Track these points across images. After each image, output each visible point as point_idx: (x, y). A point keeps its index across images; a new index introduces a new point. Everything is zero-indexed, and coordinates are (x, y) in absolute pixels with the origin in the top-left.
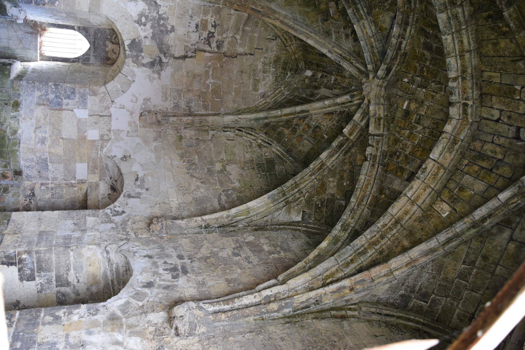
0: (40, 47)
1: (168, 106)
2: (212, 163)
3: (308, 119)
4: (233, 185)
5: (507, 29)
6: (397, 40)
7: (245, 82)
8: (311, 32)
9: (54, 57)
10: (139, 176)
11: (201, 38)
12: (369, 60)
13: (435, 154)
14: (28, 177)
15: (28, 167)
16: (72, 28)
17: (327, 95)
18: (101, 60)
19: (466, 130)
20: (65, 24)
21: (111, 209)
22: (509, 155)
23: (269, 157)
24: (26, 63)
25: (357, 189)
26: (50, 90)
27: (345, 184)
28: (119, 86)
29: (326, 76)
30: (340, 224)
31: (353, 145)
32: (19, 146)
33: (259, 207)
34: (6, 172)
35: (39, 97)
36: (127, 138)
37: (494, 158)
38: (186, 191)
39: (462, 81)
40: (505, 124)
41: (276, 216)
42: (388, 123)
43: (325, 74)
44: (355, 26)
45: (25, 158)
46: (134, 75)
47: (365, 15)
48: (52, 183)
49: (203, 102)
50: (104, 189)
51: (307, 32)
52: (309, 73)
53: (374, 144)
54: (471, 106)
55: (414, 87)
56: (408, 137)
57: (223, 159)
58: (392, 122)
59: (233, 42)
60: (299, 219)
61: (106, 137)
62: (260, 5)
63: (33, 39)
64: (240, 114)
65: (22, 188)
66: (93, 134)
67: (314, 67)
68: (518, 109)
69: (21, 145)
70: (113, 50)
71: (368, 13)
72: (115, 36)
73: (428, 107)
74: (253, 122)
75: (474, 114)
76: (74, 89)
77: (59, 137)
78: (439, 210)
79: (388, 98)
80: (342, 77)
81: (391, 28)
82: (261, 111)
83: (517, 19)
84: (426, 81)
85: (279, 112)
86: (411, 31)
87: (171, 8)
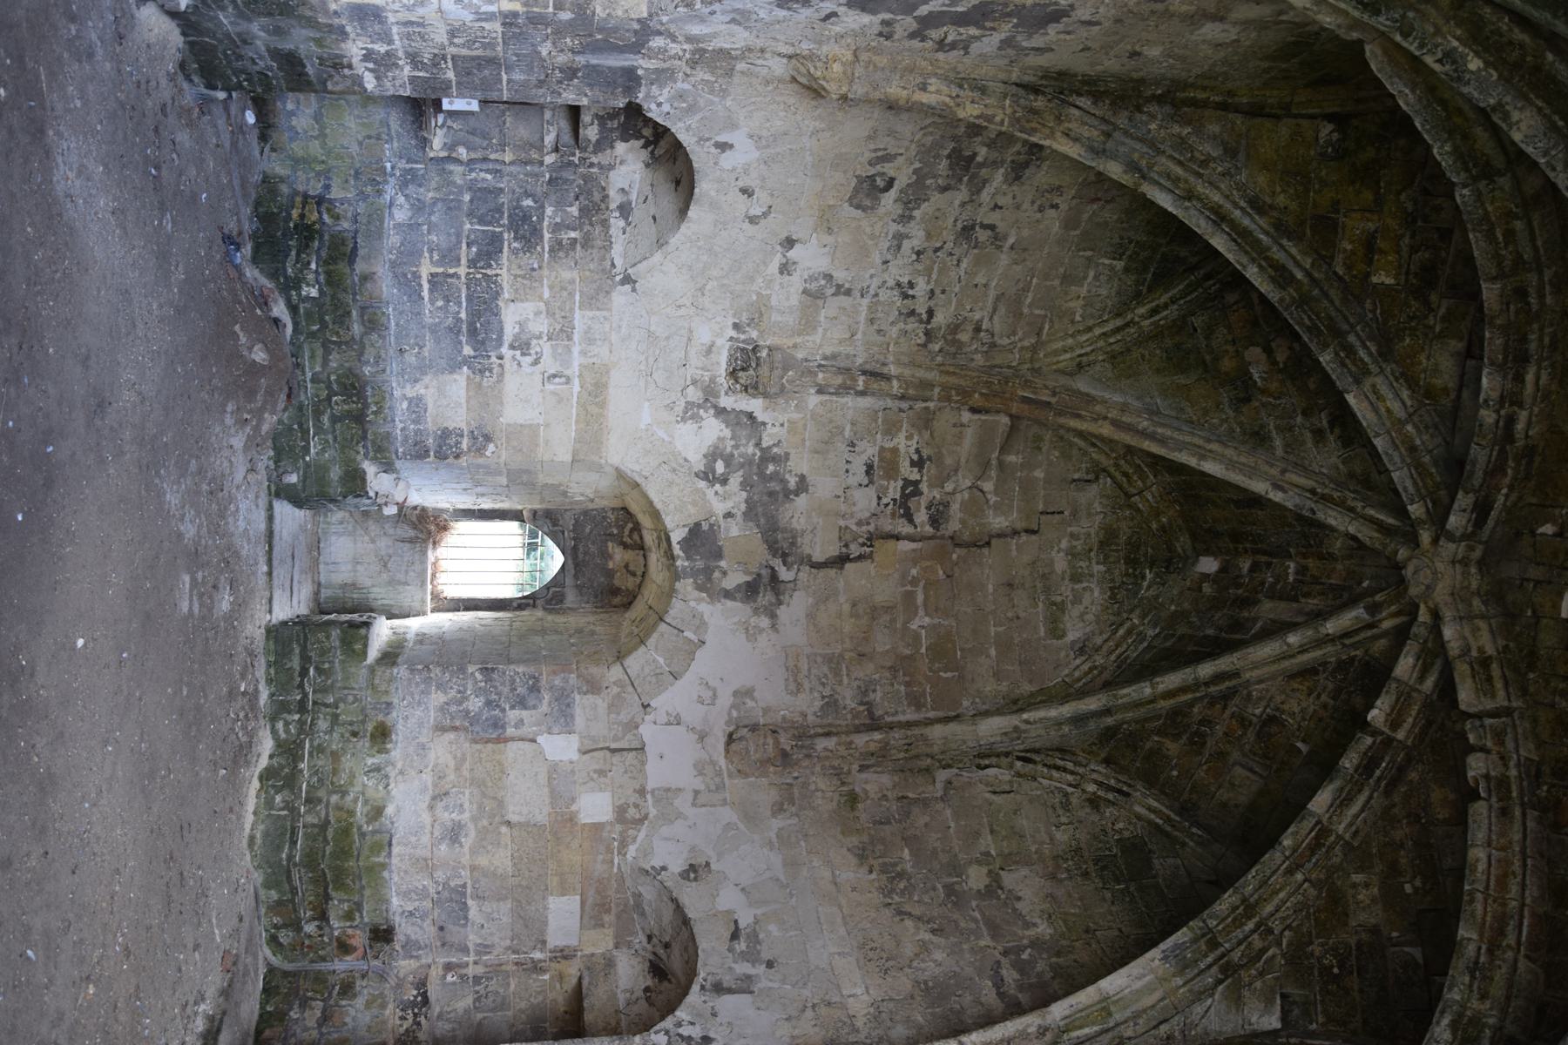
0: (434, 575)
1: (807, 704)
2: (956, 869)
3: (1237, 700)
4: (1031, 932)
6: (1497, 412)
7: (1022, 615)
8: (1209, 441)
10: (742, 925)
11: (885, 501)
12: (1411, 489)
14: (411, 947)
15: (411, 914)
20: (498, 506)
21: (667, 1033)
23: (1126, 834)
24: (396, 622)
25: (1471, 893)
26: (470, 686)
28: (661, 660)
30: (1446, 1021)
31: (1409, 759)
32: (390, 854)
33: (1139, 994)
34: (350, 931)
35: (443, 709)
38: (891, 963)
41: (1195, 1017)
43: (1264, 559)
44: (1351, 399)
45: (403, 893)
46: (702, 625)
47: (1375, 361)
48: (476, 963)
49: (908, 684)
50: (629, 974)
51: (1196, 440)
52: (1208, 565)
53: (1489, 744)
57: (988, 854)
59: (976, 504)
60: (1272, 1022)
62: (1046, 387)
64: (1022, 710)
65: (392, 981)
66: (595, 807)
69: (396, 850)
70: (626, 566)
71: (1381, 354)
72: (630, 525)
74: (1066, 729)
77: (497, 819)
79: (1496, 595)
80: (1321, 557)
82: (1082, 694)
86: (1538, 379)
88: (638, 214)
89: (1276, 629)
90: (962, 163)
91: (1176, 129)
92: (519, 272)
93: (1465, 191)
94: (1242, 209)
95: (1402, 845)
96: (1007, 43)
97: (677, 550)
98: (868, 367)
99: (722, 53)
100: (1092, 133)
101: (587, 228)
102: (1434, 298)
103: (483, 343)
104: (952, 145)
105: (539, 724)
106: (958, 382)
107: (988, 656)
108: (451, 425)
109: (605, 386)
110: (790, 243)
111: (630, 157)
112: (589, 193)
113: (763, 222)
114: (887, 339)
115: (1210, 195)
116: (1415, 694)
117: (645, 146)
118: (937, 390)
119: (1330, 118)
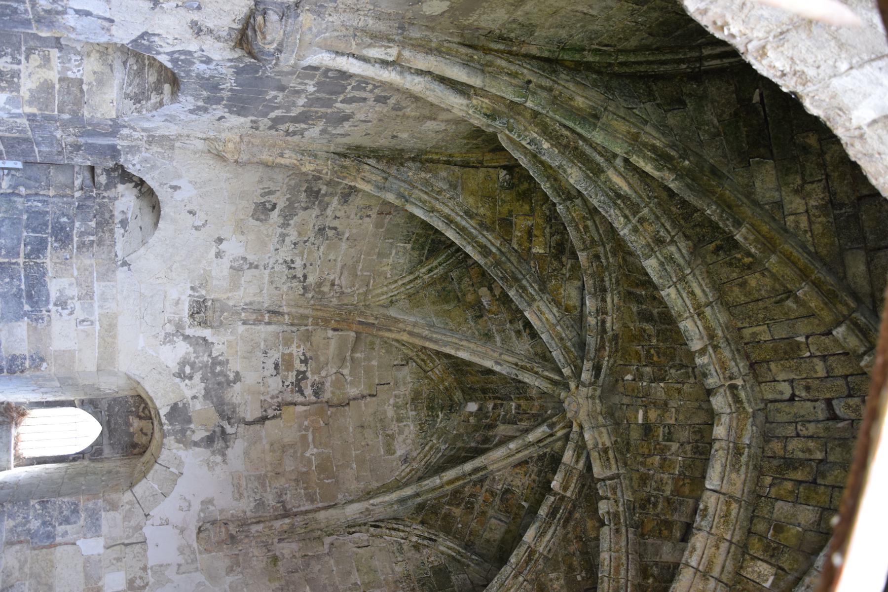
0: (16, 444)
1: (246, 506)
3: (488, 482)
5: (750, 259)
6: (596, 318)
7: (370, 443)
8: (461, 340)
9: (40, 458)
11: (287, 383)
12: (563, 361)
13: (713, 481)
16: (71, 404)
17: (510, 434)
18: (123, 449)
19: (749, 427)
20: (58, 399)
22: (832, 449)
23: (436, 563)
25: (602, 578)
26: (31, 513)
27: (579, 578)
28: (156, 486)
29: (502, 405)
31: (574, 507)
35: (12, 531)
36: (179, 576)
37: (811, 460)
39: (715, 352)
40: (804, 400)
42: (621, 453)
43: (499, 402)
44: (526, 314)
46: (181, 464)
47: (538, 294)
49: (305, 489)
51: (454, 340)
52: (472, 407)
53: (609, 495)
54: (743, 386)
55: (645, 384)
56: (662, 467)
57: (356, 584)
58: (628, 450)
59: (340, 382)
61: (139, 582)
62: (372, 315)
63: (4, 433)
64: (371, 498)
67: (479, 394)
68: (816, 372)
70: (141, 430)
72: (143, 405)
73: (677, 410)
74: (395, 507)
75: (752, 399)
76: (77, 505)
78: (754, 577)
79: (610, 414)
81: (583, 304)
82: (406, 485)
83: (756, 240)
84: (660, 370)
85: (436, 481)
87: (230, 344)
88: (132, 225)
89: (505, 440)
90: (314, 194)
91: (423, 175)
92: (57, 261)
93: (561, 207)
94: (461, 216)
95: (574, 554)
96: (323, 132)
97: (164, 420)
98: (271, 308)
99: (163, 137)
100: (377, 178)
101: (100, 234)
102: (564, 259)
103: (37, 303)
104: (307, 185)
105: (78, 533)
106: (324, 313)
107: (352, 468)
108: (18, 353)
109: (115, 325)
110: (220, 240)
111: (127, 193)
112: (103, 214)
113: (203, 229)
114: (281, 292)
115: (447, 209)
116: (574, 471)
117: (135, 187)
118: (310, 320)
119: (504, 167)
